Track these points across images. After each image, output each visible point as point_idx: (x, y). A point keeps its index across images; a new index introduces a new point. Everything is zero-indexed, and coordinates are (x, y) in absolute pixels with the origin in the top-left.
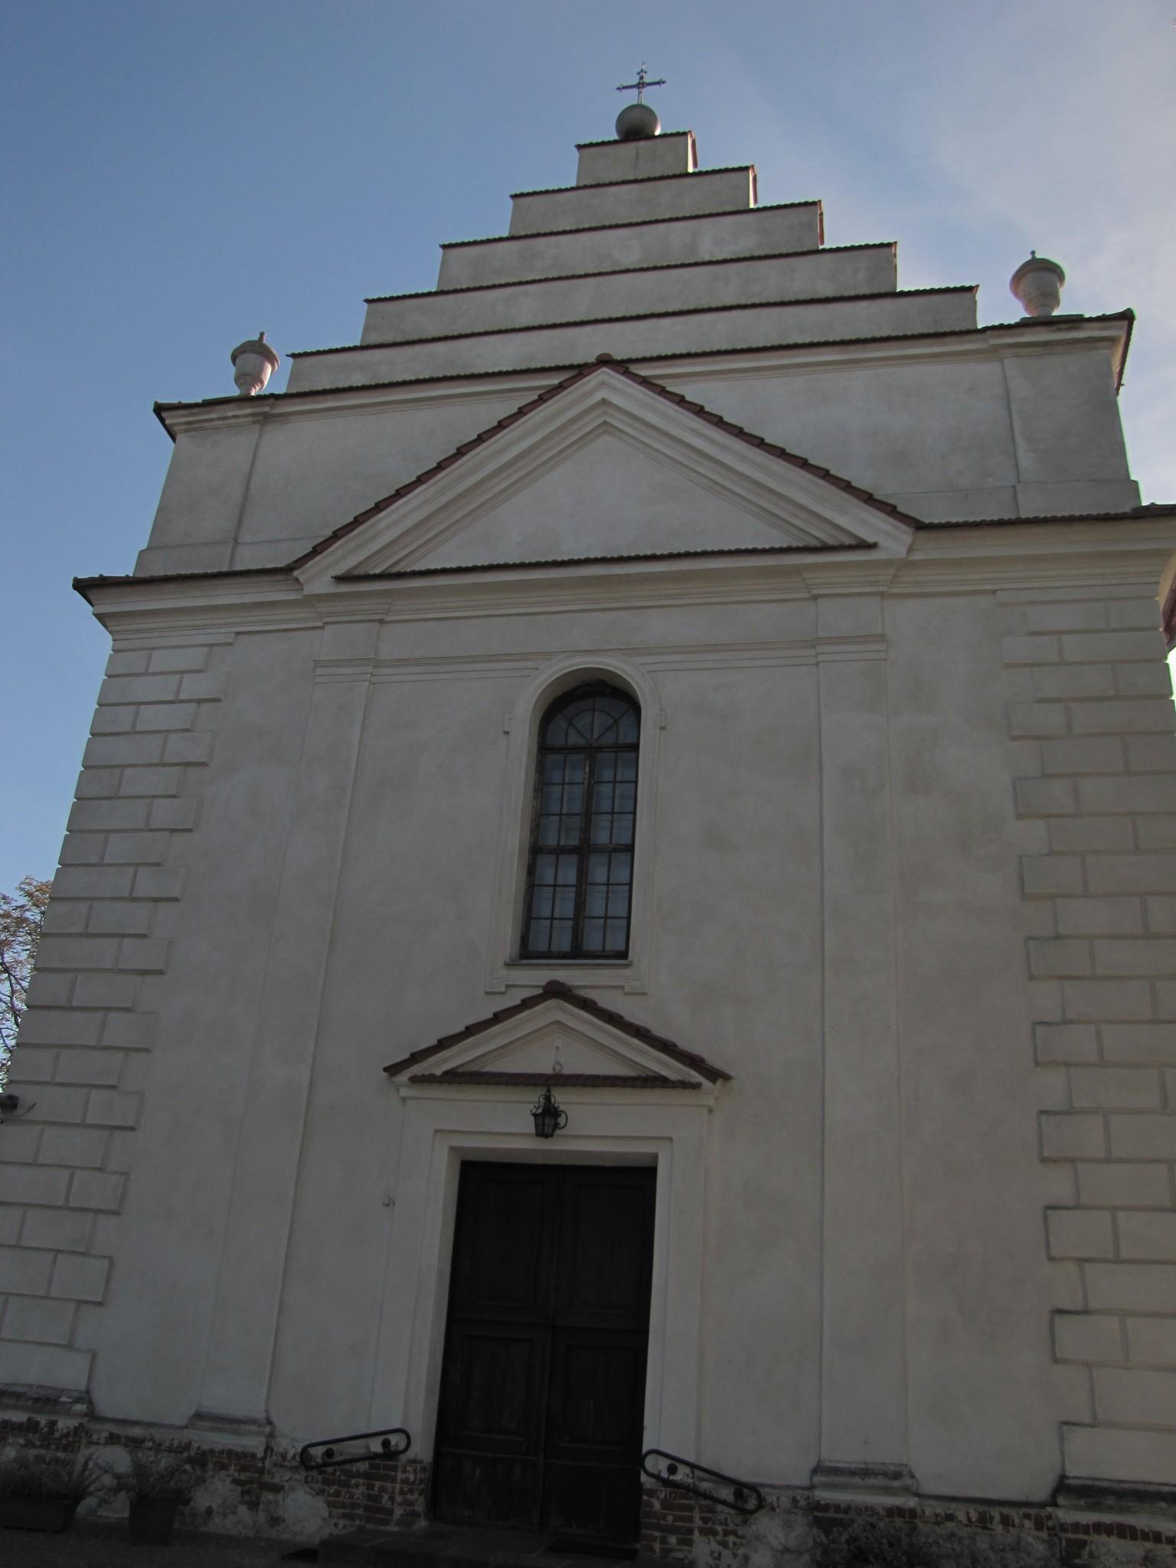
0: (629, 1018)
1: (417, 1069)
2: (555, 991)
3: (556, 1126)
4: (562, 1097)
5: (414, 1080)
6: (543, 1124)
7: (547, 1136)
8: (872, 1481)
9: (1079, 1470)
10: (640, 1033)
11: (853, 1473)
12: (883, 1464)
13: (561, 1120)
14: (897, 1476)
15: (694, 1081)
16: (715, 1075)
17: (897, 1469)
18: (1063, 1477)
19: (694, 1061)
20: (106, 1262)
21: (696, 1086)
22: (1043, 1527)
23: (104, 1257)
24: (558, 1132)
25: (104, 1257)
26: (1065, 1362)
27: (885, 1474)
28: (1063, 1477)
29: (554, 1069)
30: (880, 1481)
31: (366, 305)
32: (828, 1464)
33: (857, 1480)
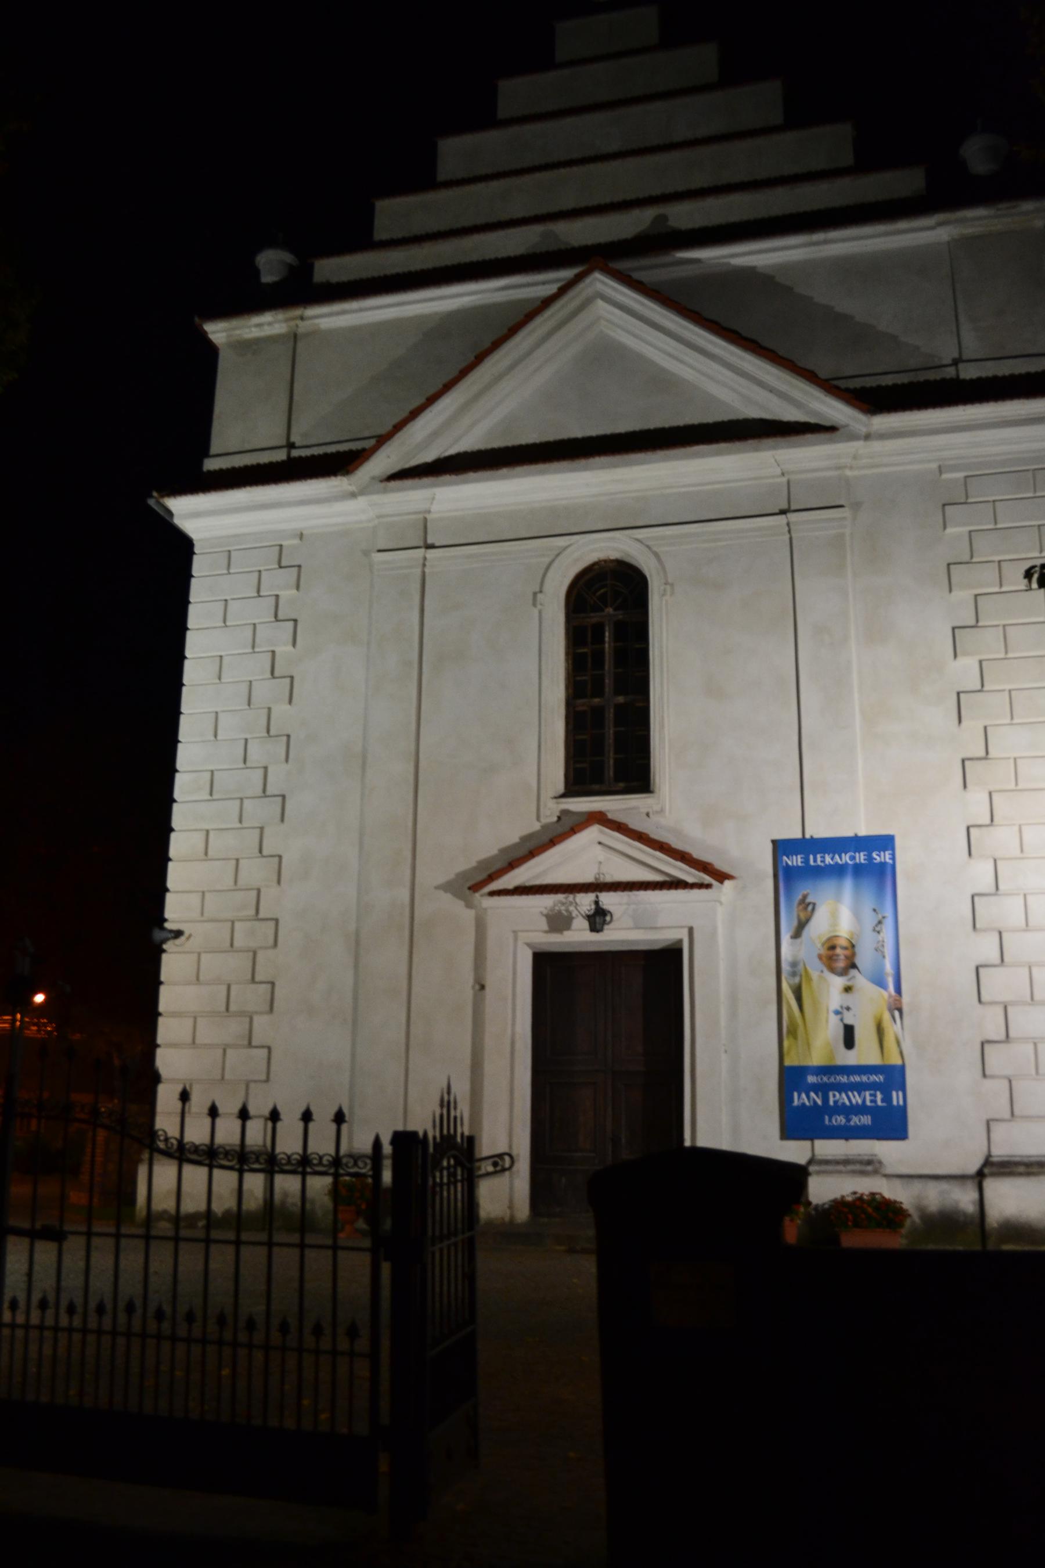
0: (653, 836)
1: (495, 886)
2: (599, 818)
3: (604, 922)
4: (263, 795)
5: (492, 894)
6: (595, 923)
7: (598, 931)
8: (850, 1168)
9: (1000, 1152)
10: (662, 847)
11: (837, 1162)
12: (859, 1155)
13: (608, 918)
14: (869, 1162)
15: (706, 882)
16: (721, 877)
17: (870, 1158)
18: (989, 1156)
19: (704, 867)
20: (266, 1051)
21: (708, 886)
22: (395, 1156)
23: (263, 1047)
24: (606, 927)
25: (263, 1047)
26: (993, 1077)
27: (861, 1162)
28: (989, 1156)
29: (596, 879)
30: (858, 1167)
31: (959, 658)
32: (820, 1157)
33: (841, 1168)
